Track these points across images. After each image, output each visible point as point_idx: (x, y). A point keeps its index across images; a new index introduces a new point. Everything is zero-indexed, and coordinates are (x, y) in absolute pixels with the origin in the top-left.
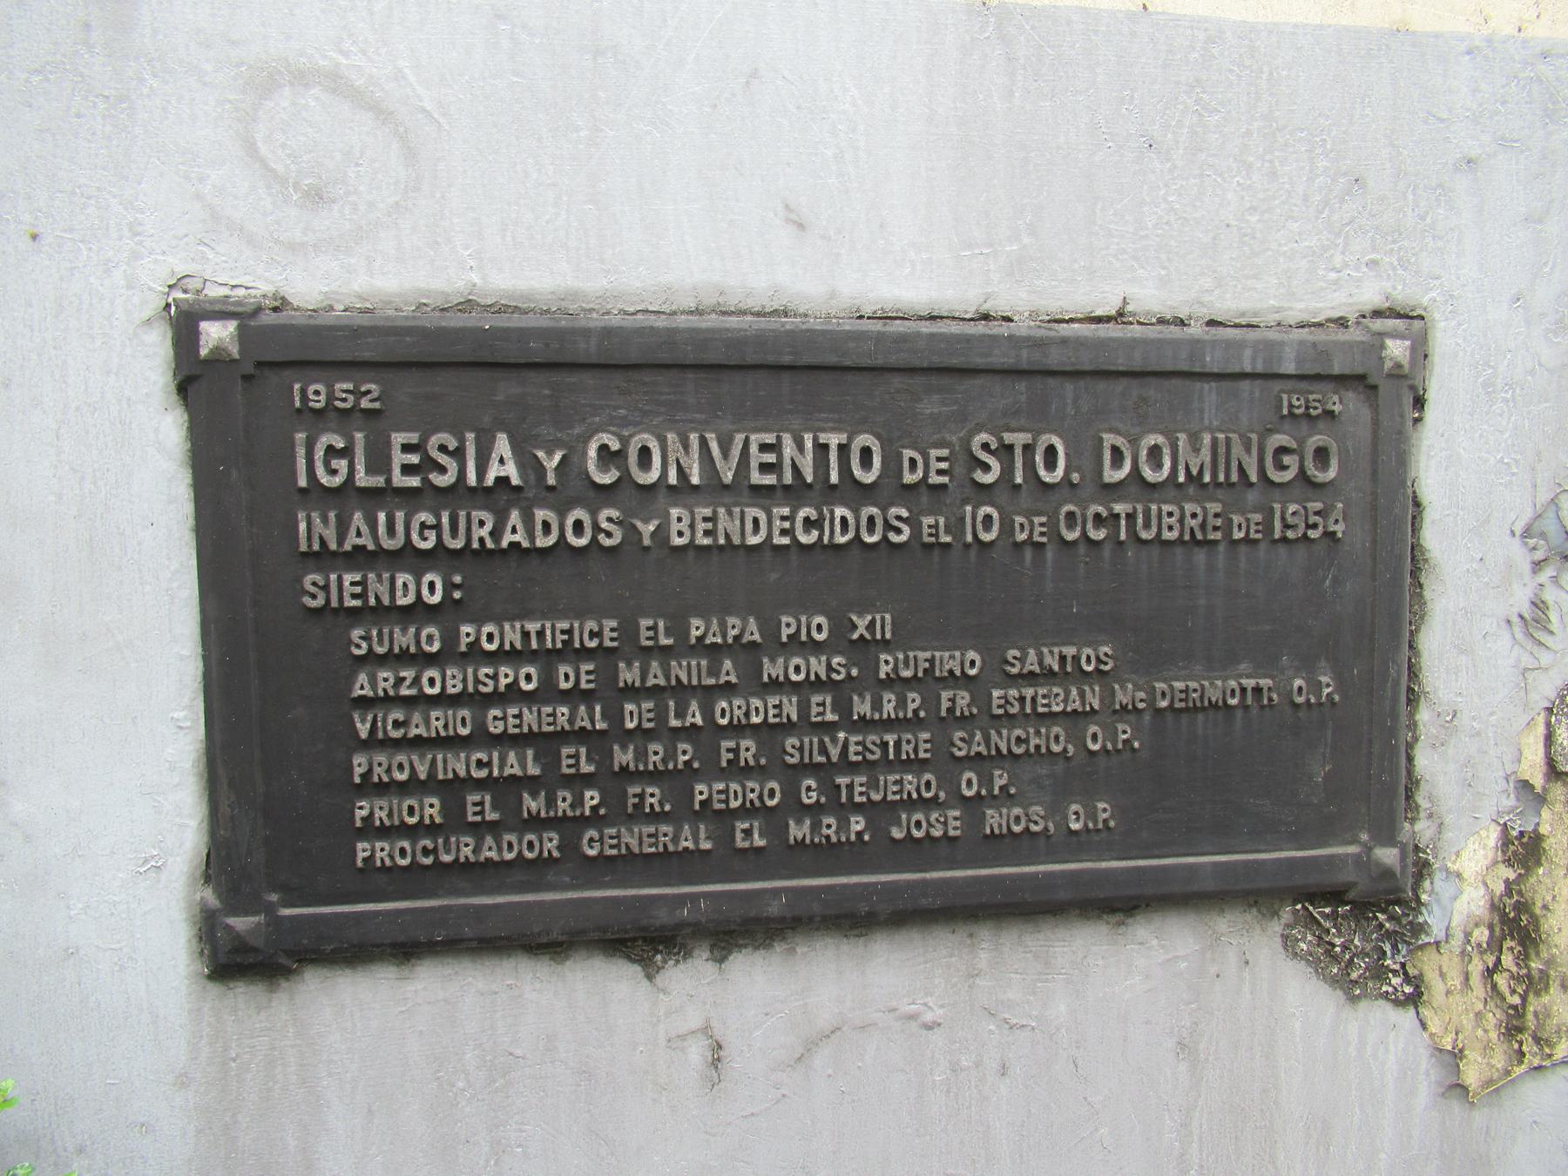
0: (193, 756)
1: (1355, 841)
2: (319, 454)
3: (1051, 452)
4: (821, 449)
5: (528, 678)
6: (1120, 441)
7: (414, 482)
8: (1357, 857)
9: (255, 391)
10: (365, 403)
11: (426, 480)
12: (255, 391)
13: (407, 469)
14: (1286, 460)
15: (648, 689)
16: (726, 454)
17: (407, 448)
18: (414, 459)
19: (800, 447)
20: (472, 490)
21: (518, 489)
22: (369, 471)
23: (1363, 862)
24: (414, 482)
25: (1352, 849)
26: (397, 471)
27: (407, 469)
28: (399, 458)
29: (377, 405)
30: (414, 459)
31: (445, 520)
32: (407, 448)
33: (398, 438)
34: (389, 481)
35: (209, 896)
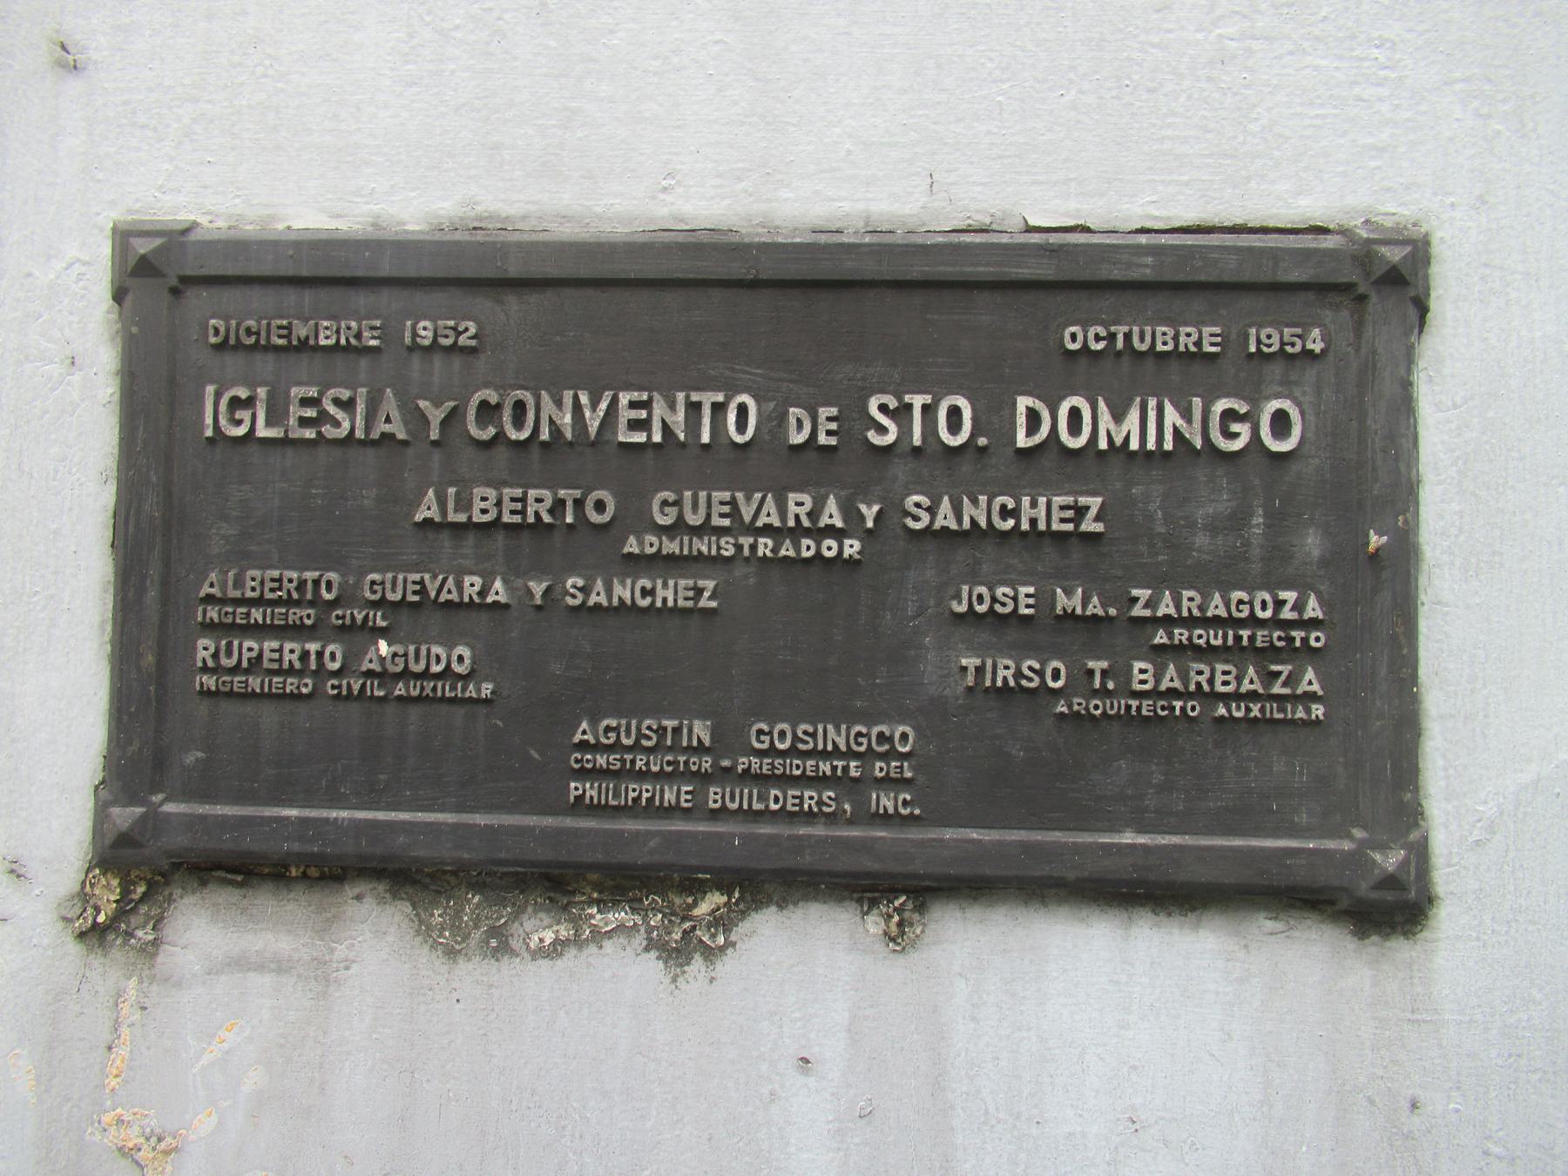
0: (97, 619)
1: (1349, 836)
2: (223, 407)
3: (955, 412)
4: (694, 408)
5: (461, 659)
6: (1039, 405)
7: (310, 434)
8: (1351, 853)
9: (162, 278)
10: (462, 340)
11: (319, 433)
12: (162, 278)
13: (304, 422)
14: (1235, 427)
15: (488, 605)
16: (594, 406)
17: (306, 402)
18: (310, 413)
19: (672, 406)
20: (360, 442)
21: (405, 443)
22: (456, 511)
23: (1358, 860)
24: (310, 434)
25: (1347, 845)
26: (292, 421)
27: (304, 422)
28: (296, 412)
29: (473, 343)
30: (310, 413)
31: (820, 730)
32: (306, 402)
33: (297, 392)
34: (470, 518)
35: (103, 794)
